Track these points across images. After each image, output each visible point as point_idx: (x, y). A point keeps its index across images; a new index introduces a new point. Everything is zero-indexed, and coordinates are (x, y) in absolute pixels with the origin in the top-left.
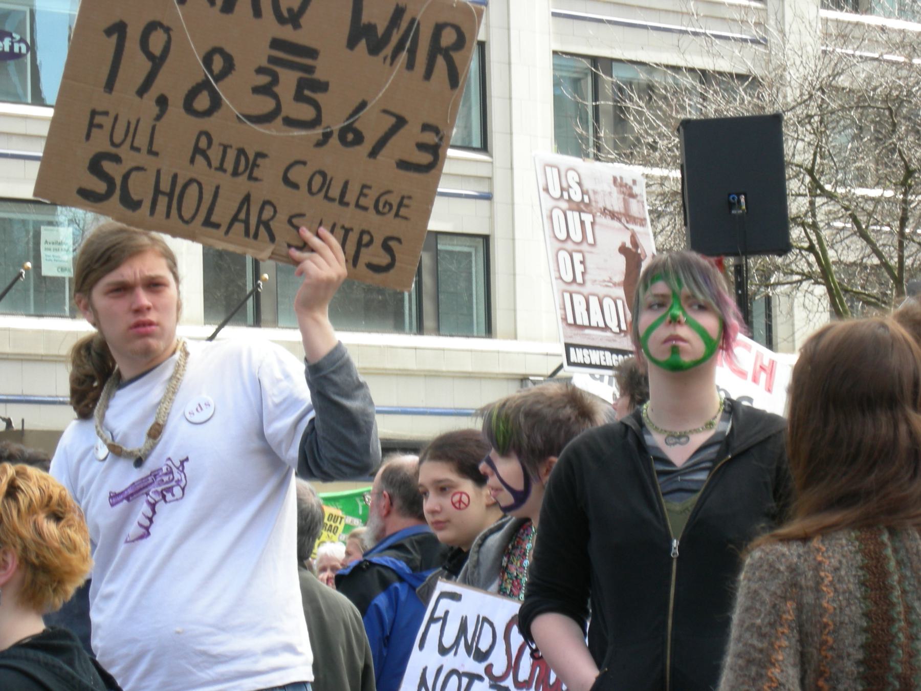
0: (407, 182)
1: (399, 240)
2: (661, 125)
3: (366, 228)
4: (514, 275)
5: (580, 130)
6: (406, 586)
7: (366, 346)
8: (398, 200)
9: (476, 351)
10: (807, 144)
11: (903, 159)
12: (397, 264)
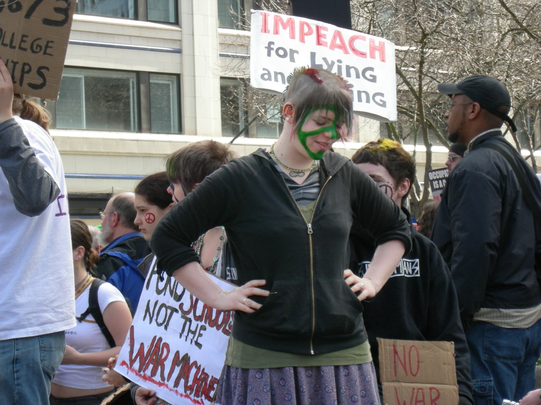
0: (50, 32)
1: (47, 69)
2: (280, 8)
3: (26, 62)
4: (195, 97)
5: (232, 12)
6: (129, 268)
7: (108, 139)
8: (45, 43)
9: (173, 142)
10: (364, 19)
11: (421, 28)
12: (47, 83)
